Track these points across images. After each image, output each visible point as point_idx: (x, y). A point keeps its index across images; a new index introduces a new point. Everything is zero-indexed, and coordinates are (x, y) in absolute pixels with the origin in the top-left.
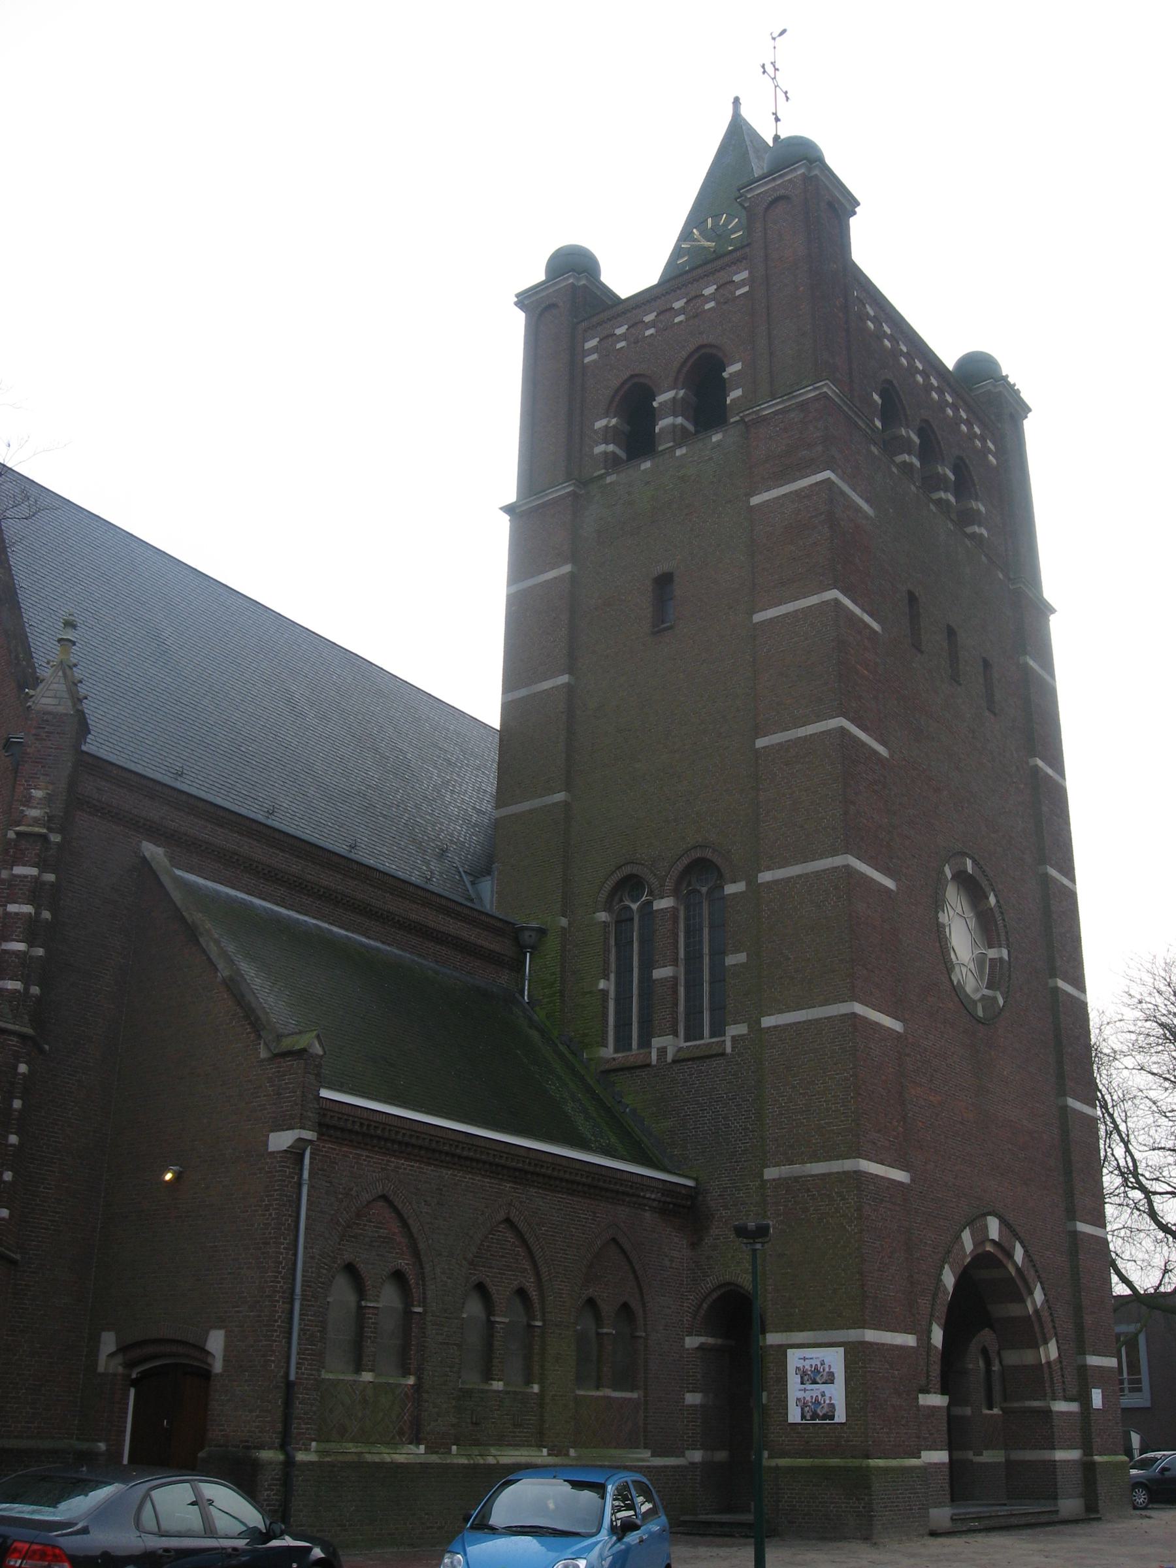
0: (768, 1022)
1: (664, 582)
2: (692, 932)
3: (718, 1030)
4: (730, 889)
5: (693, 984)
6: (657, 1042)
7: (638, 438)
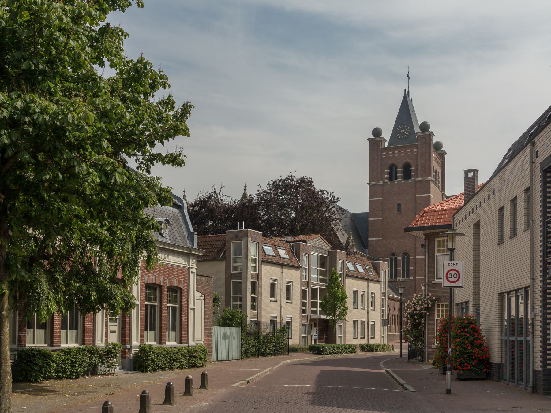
0: (417, 278)
1: (399, 205)
2: (403, 263)
3: (408, 277)
4: (411, 258)
5: (403, 270)
6: (398, 278)
7: (393, 176)
